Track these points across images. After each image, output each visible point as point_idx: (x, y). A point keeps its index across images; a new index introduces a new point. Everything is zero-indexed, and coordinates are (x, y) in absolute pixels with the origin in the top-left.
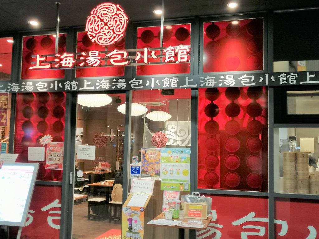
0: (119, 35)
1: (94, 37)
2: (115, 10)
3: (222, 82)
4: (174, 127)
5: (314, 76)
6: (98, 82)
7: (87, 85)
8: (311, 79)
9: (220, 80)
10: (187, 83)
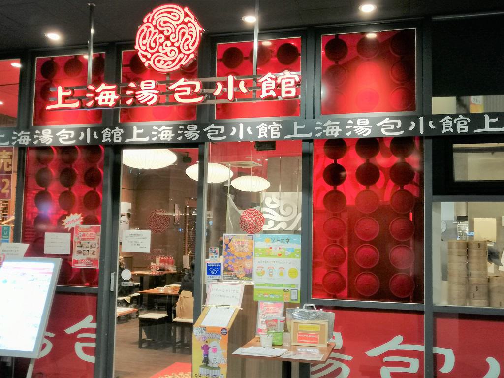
0: (188, 55)
1: (148, 59)
2: (182, 16)
3: (352, 129)
4: (275, 200)
5: (496, 120)
6: (155, 130)
7: (138, 134)
8: (492, 125)
9: (348, 127)
10: (296, 131)
